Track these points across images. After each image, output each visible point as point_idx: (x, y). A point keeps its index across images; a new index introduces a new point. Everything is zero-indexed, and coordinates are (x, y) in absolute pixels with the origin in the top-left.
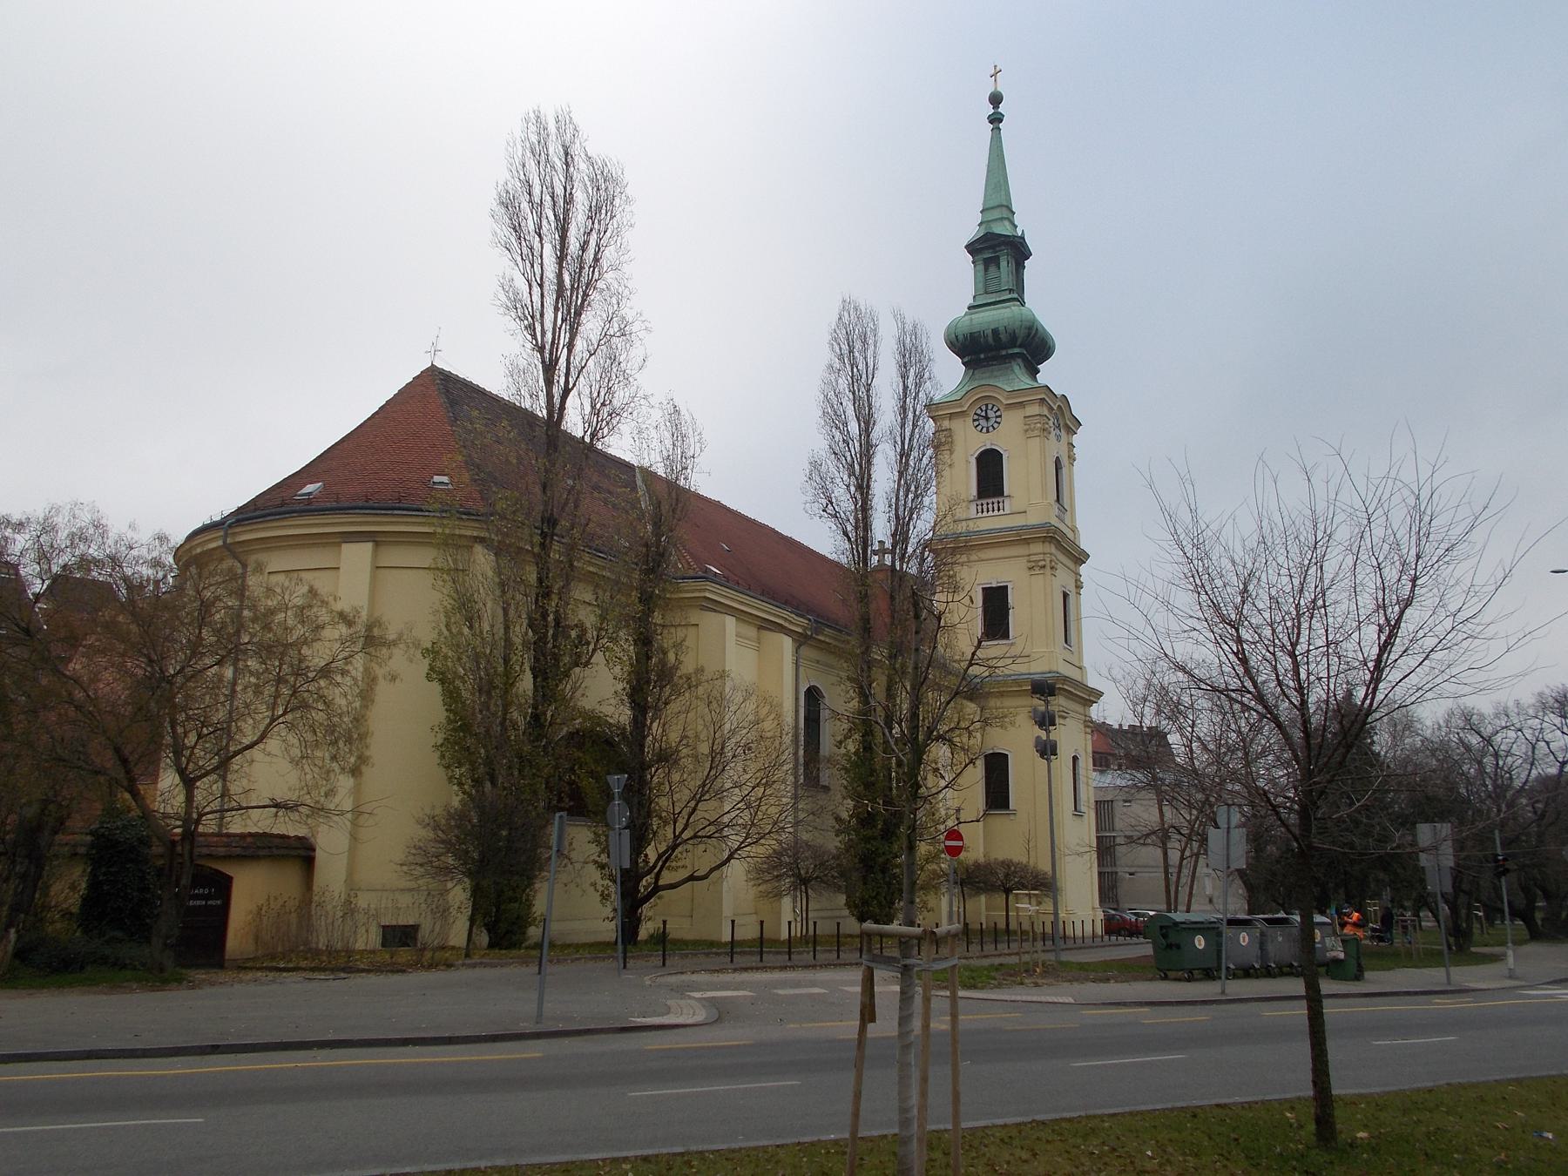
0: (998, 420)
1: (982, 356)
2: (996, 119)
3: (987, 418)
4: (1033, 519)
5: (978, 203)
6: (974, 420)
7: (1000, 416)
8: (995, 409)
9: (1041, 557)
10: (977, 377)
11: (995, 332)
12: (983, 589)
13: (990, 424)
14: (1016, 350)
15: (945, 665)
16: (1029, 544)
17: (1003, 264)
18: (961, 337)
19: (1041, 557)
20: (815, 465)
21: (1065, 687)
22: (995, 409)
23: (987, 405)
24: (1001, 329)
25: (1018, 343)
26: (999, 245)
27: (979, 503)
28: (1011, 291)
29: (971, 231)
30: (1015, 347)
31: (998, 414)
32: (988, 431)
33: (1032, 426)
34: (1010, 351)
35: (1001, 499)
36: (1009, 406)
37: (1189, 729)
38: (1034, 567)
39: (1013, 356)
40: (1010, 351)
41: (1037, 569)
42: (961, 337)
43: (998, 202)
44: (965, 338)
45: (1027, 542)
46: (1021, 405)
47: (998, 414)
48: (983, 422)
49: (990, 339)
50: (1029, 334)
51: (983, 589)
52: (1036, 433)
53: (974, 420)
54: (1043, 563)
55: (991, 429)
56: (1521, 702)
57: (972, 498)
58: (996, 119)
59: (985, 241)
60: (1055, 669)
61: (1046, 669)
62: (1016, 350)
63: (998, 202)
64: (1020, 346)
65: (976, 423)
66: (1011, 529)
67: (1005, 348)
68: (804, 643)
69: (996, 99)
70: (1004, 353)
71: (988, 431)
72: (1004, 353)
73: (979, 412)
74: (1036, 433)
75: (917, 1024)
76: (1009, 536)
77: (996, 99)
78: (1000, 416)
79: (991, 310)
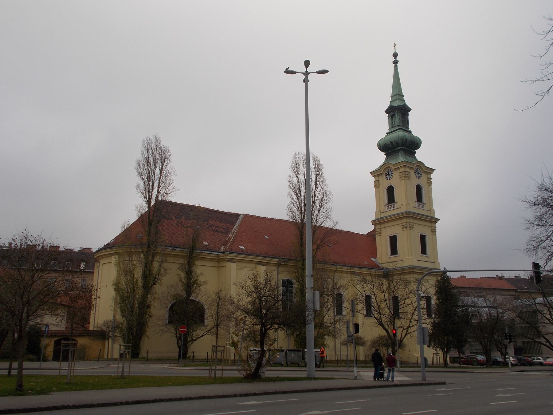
0: (392, 175)
1: (390, 152)
2: (395, 62)
3: (389, 175)
4: (403, 210)
5: (390, 94)
6: (385, 176)
7: (393, 174)
8: (391, 171)
9: (405, 224)
10: (389, 159)
11: (392, 142)
12: (390, 237)
13: (390, 177)
14: (400, 148)
15: (379, 267)
16: (402, 219)
17: (396, 116)
18: (381, 146)
19: (405, 224)
20: (289, 207)
21: (414, 271)
22: (391, 171)
23: (389, 170)
24: (393, 141)
25: (400, 145)
26: (395, 109)
27: (389, 205)
28: (399, 126)
29: (387, 106)
30: (399, 146)
31: (392, 172)
32: (389, 179)
33: (402, 176)
34: (398, 148)
35: (394, 204)
36: (395, 169)
37: (395, 283)
38: (404, 227)
39: (400, 150)
40: (398, 148)
41: (404, 228)
42: (381, 146)
43: (397, 93)
44: (383, 146)
45: (401, 219)
46: (398, 168)
47: (392, 172)
48: (388, 176)
49: (390, 145)
50: (403, 142)
51: (390, 237)
52: (403, 178)
53: (385, 176)
54: (406, 226)
55: (390, 178)
56: (384, 267)
57: (386, 204)
58: (395, 62)
59: (390, 109)
60: (411, 264)
61: (408, 265)
62: (400, 148)
63: (397, 93)
64: (401, 146)
65: (386, 177)
66: (396, 214)
67: (396, 148)
68: (279, 266)
69: (395, 55)
70: (396, 149)
71: (389, 179)
72: (396, 149)
73: (387, 173)
74: (403, 178)
75: (210, 375)
76: (395, 217)
77: (395, 55)
78: (393, 174)
79: (393, 134)
